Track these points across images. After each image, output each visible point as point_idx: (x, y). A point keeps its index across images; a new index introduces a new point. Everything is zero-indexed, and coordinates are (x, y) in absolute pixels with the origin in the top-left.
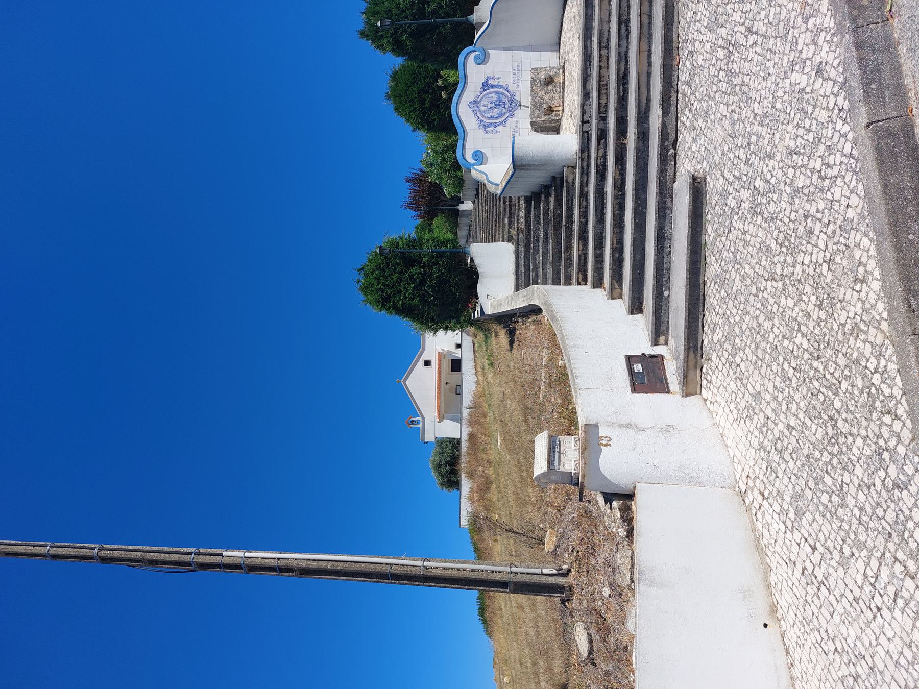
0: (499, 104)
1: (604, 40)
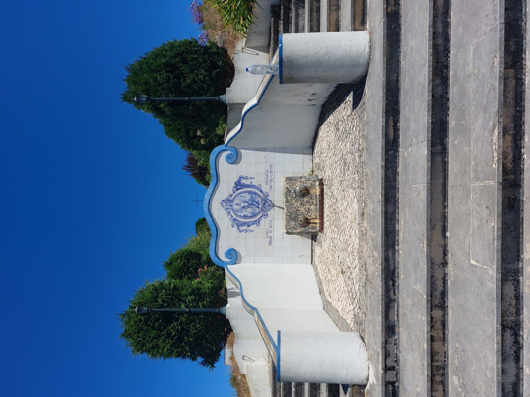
0: (252, 203)
1: (438, 293)
